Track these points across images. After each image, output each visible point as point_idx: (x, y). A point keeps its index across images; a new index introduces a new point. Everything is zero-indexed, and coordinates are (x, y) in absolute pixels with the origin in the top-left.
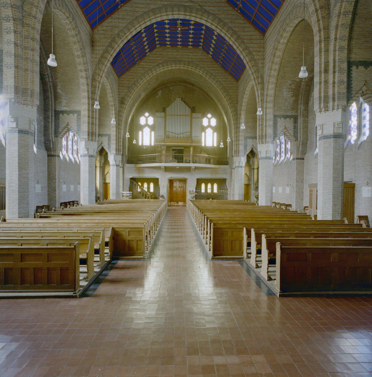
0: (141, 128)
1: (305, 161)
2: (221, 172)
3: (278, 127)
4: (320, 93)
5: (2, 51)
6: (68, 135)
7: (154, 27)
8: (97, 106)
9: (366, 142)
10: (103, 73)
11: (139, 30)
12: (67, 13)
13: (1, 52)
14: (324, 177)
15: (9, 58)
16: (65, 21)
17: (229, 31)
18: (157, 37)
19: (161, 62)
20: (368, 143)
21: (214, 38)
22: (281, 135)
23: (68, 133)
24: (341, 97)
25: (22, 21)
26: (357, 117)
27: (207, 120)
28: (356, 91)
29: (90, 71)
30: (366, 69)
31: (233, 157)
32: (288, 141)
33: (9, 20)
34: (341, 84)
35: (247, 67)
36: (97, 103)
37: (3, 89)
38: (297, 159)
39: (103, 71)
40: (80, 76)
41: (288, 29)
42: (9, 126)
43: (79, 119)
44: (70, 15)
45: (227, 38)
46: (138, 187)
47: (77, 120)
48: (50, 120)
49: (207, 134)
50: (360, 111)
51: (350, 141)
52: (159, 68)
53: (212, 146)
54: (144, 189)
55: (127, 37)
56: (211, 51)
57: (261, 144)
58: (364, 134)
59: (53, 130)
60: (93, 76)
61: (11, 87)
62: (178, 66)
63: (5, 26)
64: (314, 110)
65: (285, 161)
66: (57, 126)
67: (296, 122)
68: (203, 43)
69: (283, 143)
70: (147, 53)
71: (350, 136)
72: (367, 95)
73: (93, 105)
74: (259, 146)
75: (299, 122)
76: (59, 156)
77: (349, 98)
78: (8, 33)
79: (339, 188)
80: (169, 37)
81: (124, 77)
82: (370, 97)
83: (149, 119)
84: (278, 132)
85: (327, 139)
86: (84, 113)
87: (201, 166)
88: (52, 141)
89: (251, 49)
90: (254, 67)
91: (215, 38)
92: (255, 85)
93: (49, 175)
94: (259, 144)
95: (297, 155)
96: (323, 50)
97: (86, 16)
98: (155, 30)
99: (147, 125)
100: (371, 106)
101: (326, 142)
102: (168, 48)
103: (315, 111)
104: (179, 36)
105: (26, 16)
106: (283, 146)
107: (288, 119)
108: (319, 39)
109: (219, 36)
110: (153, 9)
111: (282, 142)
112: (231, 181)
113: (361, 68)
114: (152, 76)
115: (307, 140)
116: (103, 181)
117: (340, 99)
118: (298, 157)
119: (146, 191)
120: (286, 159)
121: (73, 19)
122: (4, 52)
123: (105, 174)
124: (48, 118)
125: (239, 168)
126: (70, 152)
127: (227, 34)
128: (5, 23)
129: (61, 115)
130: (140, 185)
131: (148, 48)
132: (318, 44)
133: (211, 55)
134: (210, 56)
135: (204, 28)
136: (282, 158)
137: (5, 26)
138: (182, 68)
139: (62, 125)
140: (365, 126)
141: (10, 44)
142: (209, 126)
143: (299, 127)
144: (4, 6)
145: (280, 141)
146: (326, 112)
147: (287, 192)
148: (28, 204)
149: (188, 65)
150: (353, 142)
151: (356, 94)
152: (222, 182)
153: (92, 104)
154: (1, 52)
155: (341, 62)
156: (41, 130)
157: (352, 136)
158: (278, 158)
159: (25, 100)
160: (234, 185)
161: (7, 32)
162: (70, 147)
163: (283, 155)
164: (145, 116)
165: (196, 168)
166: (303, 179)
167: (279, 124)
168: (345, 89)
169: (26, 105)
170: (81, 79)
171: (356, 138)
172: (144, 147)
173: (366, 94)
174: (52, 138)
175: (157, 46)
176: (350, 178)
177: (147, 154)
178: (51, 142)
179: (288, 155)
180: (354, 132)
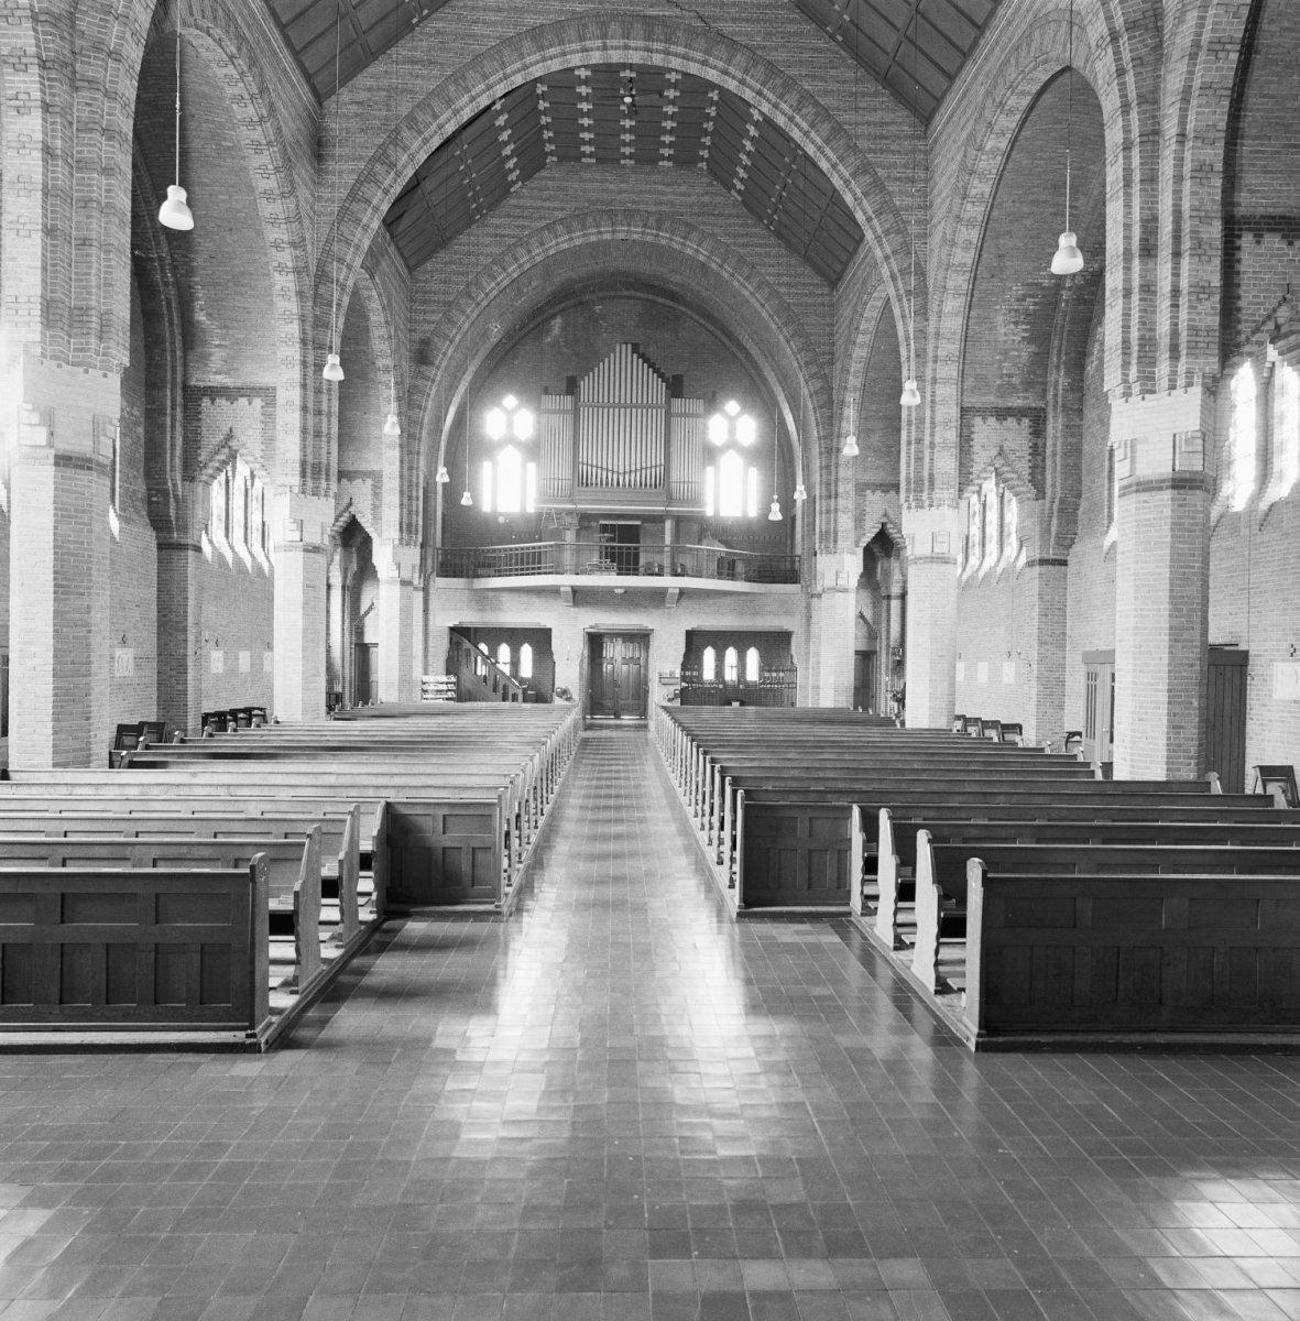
1: (1071, 569)
2: (773, 607)
4: (1126, 327)
6: (230, 474)
8: (333, 372)
11: (484, 101)
15: (23, 200)
16: (224, 71)
19: (560, 215)
22: (985, 479)
23: (229, 468)
28: (1255, 321)
33: (26, 65)
34: (1201, 296)
35: (869, 235)
36: (333, 359)
38: (1043, 562)
43: (269, 418)
44: (239, 49)
54: (500, 666)
61: (29, 301)
66: (192, 443)
67: (1038, 431)
73: (319, 367)
75: (1050, 431)
76: (198, 549)
79: (1192, 666)
83: (516, 417)
84: (976, 469)
86: (289, 395)
88: (175, 496)
89: (881, 172)
91: (753, 131)
94: (909, 508)
96: (1137, 177)
101: (1145, 502)
107: (1011, 422)
112: (808, 639)
114: (528, 266)
117: (1197, 351)
118: (1046, 557)
123: (362, 612)
128: (9, 74)
129: (206, 402)
135: (714, 95)
136: (990, 561)
138: (636, 237)
139: (210, 439)
141: (27, 151)
143: (1049, 450)
145: (983, 498)
146: (1147, 396)
147: (1005, 680)
155: (1200, 218)
158: (974, 560)
164: (505, 410)
166: (1064, 634)
168: (1215, 314)
169: (81, 369)
170: (276, 274)
174: (174, 485)
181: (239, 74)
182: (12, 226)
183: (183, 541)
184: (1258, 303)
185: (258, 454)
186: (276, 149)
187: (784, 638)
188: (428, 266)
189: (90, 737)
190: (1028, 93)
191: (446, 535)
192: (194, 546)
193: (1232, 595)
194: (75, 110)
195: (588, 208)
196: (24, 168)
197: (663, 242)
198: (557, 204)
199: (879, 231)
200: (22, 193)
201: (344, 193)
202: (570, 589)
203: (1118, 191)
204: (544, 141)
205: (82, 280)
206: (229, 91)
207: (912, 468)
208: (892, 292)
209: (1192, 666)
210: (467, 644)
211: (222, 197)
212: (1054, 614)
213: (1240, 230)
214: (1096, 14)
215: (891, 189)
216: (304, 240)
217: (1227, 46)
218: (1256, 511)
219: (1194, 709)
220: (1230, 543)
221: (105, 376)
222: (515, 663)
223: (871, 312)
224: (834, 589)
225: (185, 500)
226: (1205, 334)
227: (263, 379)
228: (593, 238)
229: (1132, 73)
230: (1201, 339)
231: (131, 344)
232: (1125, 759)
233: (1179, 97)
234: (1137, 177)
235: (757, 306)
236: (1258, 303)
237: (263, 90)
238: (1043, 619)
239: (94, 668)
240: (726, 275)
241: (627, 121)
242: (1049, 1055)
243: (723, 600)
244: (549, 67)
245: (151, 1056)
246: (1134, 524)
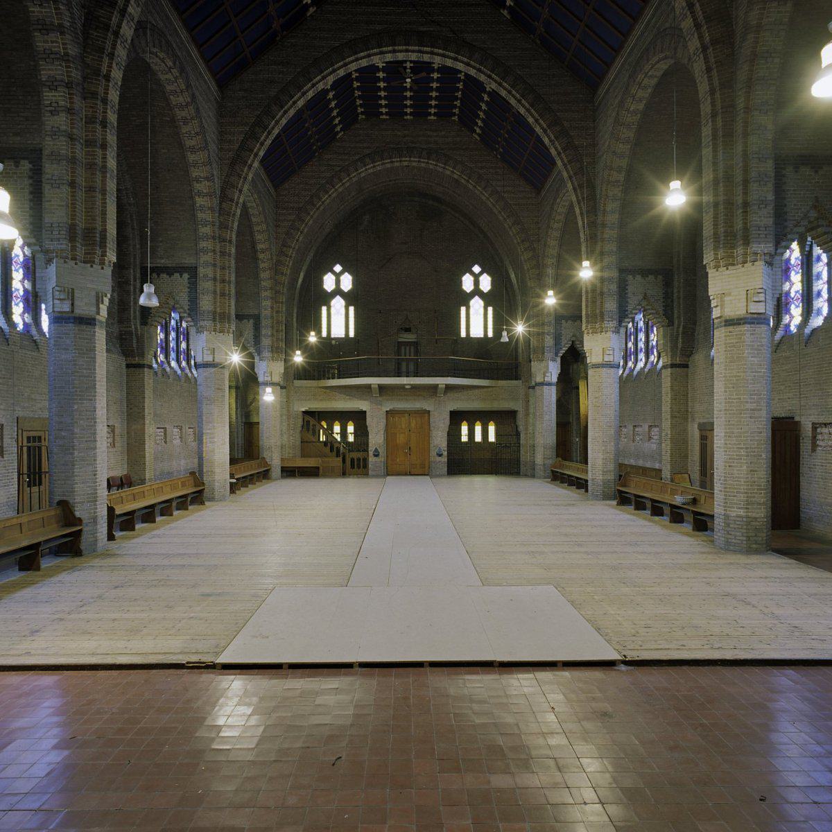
0: (326, 298)
1: (691, 369)
2: (501, 394)
3: (630, 295)
4: (716, 225)
5: (41, 150)
7: (358, 103)
9: (821, 330)
10: (244, 183)
12: (168, 60)
13: (39, 152)
14: (728, 410)
15: (55, 166)
16: (167, 76)
17: (517, 85)
18: (360, 97)
19: (368, 152)
20: (825, 332)
21: (477, 131)
22: (636, 314)
24: (761, 236)
25: (81, 86)
26: (802, 275)
27: (472, 278)
28: (795, 220)
29: (216, 179)
30: (816, 172)
31: (530, 362)
32: (652, 327)
33: (56, 86)
34: (761, 206)
35: (559, 163)
37: (44, 231)
38: (672, 366)
39: (245, 178)
40: (196, 191)
41: (646, 81)
42: (55, 310)
44: (174, 64)
45: (513, 102)
46: (321, 430)
47: (189, 288)
48: (132, 288)
49: (472, 311)
50: (807, 262)
51: (788, 326)
52: (365, 166)
53: (482, 336)
54: (335, 435)
55: (295, 103)
56: (477, 126)
57: (590, 335)
58: (819, 312)
59: (240, 436)
60: (223, 190)
61: (59, 226)
62: (406, 161)
63: (48, 100)
64: (704, 263)
65: (646, 370)
67: (668, 284)
68: (461, 99)
69: (641, 330)
70: (338, 133)
71: (788, 316)
72: (819, 230)
74: (586, 338)
75: (676, 284)
76: (150, 367)
77: (781, 242)
78: (53, 113)
79: (761, 433)
80: (386, 106)
81: (287, 187)
82: (825, 233)
83: (342, 278)
84: (630, 308)
85: (731, 327)
87: (460, 383)
88: (137, 335)
89: (566, 124)
90: (573, 164)
92: (575, 204)
93: (131, 409)
94: (588, 333)
95: (672, 357)
96: (720, 133)
97: (209, 61)
98: (355, 82)
99: (338, 291)
100: (831, 253)
101: (730, 332)
102: (385, 120)
103: (705, 266)
104: (408, 94)
105: (89, 76)
106: (642, 336)
107: (651, 278)
108: (712, 110)
109: (493, 94)
110: (350, 41)
111: (639, 327)
112: (527, 415)
113: (806, 171)
114: (348, 184)
115: (695, 325)
116: (244, 420)
117: (759, 240)
118: (675, 362)
119: (339, 440)
120: (649, 366)
121: (182, 70)
122: (46, 152)
123: (249, 403)
124: (127, 283)
125: (545, 387)
126: (173, 355)
127: (514, 92)
128: (46, 92)
130: (325, 427)
131: (337, 116)
132: (710, 120)
133: (479, 135)
134: (476, 137)
136: (641, 365)
137: (48, 100)
138: (414, 164)
140: (819, 294)
141: (57, 137)
142: (477, 292)
143: (675, 295)
144: (56, 81)
146: (729, 267)
148: (95, 475)
149: (428, 159)
150: (793, 329)
151: (796, 226)
152: (505, 418)
153: (221, 252)
154: (39, 152)
155: (759, 159)
156: (114, 310)
157: (792, 317)
158: (630, 364)
159: (89, 253)
160: (534, 425)
161: (51, 112)
162: (172, 344)
163: (642, 356)
164: (334, 273)
165: (449, 388)
166: (687, 411)
167: (630, 289)
168: (770, 217)
169: (89, 265)
170: (197, 197)
171: (801, 321)
172: (333, 342)
173: (818, 226)
174: (136, 328)
175: (359, 118)
176: (789, 410)
177: (340, 358)
178: (134, 337)
179: (653, 356)
180: (797, 307)
181: (174, 77)
182: (48, 181)
183: (141, 362)
184: (797, 209)
185: (186, 308)
186: (196, 122)
187: (512, 414)
188: (286, 186)
189: (96, 486)
190: (656, 77)
191: (413, 471)
192: (148, 365)
193: (790, 386)
194: (84, 111)
195: (385, 146)
196: (55, 147)
197: (431, 167)
198: (365, 145)
199: (566, 161)
200: (54, 162)
201: (236, 146)
202: (377, 386)
203: (709, 142)
204: (357, 106)
205: (89, 212)
206: (169, 88)
207: (589, 309)
208: (574, 198)
209: (761, 433)
210: (312, 422)
211: (163, 151)
212: (682, 398)
213: (785, 164)
214: (693, 34)
215: (572, 134)
216: (213, 175)
217: (773, 55)
218: (803, 333)
219: (763, 459)
220: (788, 354)
221: (102, 268)
222: (344, 433)
223: (562, 210)
224: (542, 384)
225: (142, 335)
226: (764, 229)
227: (189, 261)
228: (388, 166)
229: (715, 70)
230: (762, 232)
231: (117, 249)
232: (721, 491)
233: (745, 85)
234: (720, 133)
235: (490, 205)
236: (797, 209)
237: (188, 86)
238: (674, 401)
239: (98, 444)
240: (471, 187)
241: (408, 109)
242: (667, 667)
243: (470, 392)
244: (360, 65)
245: (154, 671)
246: (724, 346)
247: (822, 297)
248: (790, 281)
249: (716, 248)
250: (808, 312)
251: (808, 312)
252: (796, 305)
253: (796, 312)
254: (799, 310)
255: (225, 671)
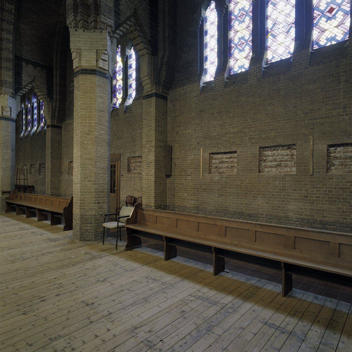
51: (115, 104)
58: (131, 95)
71: (115, 99)
157: (117, 81)
171: (121, 58)
180: (120, 93)
247: (132, 88)
248: (116, 97)
249: (76, 13)
250: (126, 96)
251: (126, 96)
252: (119, 93)
253: (120, 96)
254: (121, 77)
255: (281, 261)
